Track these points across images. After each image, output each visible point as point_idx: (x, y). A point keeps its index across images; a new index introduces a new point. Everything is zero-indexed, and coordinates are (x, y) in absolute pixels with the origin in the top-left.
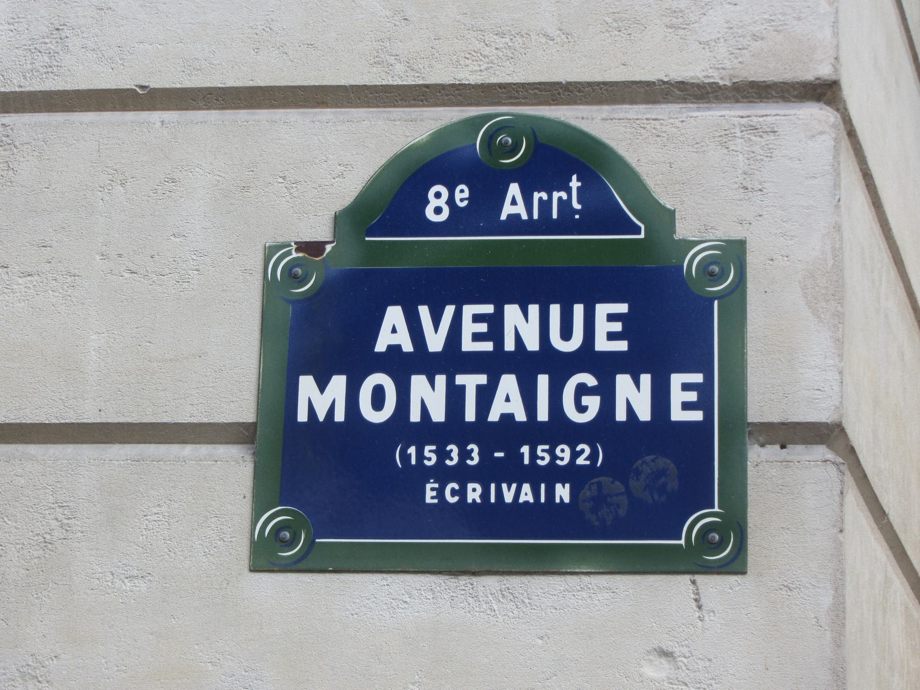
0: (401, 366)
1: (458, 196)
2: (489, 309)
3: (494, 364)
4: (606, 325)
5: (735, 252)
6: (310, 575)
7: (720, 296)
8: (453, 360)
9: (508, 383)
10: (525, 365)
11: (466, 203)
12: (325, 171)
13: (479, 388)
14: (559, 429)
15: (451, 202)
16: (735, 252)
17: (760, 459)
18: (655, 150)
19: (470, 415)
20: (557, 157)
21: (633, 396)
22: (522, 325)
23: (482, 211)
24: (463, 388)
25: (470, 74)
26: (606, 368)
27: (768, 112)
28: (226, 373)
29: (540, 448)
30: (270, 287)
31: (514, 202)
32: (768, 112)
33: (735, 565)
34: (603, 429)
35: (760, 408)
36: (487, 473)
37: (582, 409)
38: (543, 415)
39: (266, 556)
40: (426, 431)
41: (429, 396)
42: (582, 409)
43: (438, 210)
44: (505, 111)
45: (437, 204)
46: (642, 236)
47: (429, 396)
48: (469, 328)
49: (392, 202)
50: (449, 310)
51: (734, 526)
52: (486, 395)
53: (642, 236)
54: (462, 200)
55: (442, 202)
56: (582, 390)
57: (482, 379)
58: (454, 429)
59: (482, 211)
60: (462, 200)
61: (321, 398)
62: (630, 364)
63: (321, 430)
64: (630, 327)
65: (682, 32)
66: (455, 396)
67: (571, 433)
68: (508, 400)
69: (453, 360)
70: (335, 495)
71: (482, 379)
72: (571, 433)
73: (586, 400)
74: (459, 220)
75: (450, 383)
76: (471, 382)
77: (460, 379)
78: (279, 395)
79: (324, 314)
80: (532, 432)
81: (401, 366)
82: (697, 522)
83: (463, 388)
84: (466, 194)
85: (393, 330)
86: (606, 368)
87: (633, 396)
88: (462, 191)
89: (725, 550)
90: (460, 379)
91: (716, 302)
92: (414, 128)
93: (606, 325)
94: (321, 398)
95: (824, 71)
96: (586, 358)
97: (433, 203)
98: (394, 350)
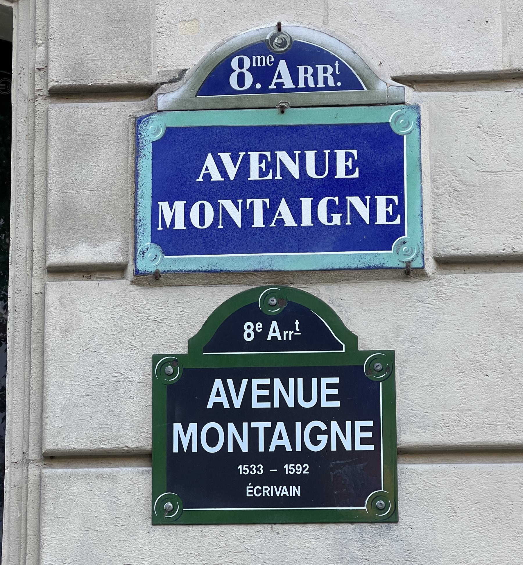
1: (257, 327)
2: (267, 381)
4: (324, 390)
6: (265, 529)
7: (383, 380)
9: (280, 426)
11: (261, 330)
13: (265, 429)
15: (254, 330)
19: (261, 449)
24: (327, 395)
29: (290, 465)
35: (406, 437)
37: (316, 443)
38: (298, 448)
42: (316, 443)
43: (249, 335)
45: (250, 331)
46: (344, 351)
48: (255, 393)
50: (245, 382)
52: (269, 433)
53: (344, 351)
54: (259, 329)
55: (251, 331)
56: (316, 431)
57: (269, 425)
60: (259, 329)
61: (186, 436)
63: (185, 456)
66: (253, 433)
71: (269, 425)
73: (319, 437)
75: (249, 425)
76: (261, 426)
77: (254, 425)
81: (222, 415)
83: (327, 395)
84: (261, 326)
85: (219, 394)
88: (259, 325)
90: (254, 425)
91: (381, 383)
93: (324, 390)
94: (186, 436)
95: (403, 100)
96: (318, 413)
97: (247, 331)
98: (218, 406)
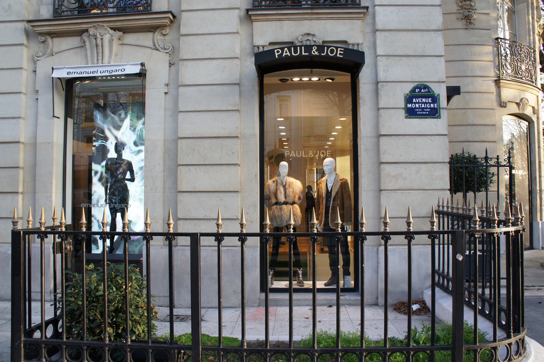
0: (415, 103)
3: (422, 103)
5: (439, 95)
8: (419, 103)
10: (424, 103)
12: (408, 88)
14: (427, 108)
16: (439, 95)
17: (441, 110)
18: (433, 86)
20: (426, 87)
21: (432, 105)
22: (424, 100)
23: (420, 91)
25: (418, 80)
26: (430, 103)
27: (538, 188)
28: (402, 104)
30: (405, 97)
31: (422, 91)
32: (538, 188)
33: (440, 118)
34: (430, 108)
36: (422, 111)
39: (406, 117)
40: (417, 108)
41: (417, 105)
44: (421, 83)
45: (417, 91)
47: (417, 105)
49: (413, 90)
51: (440, 115)
58: (419, 108)
59: (420, 91)
61: (409, 106)
62: (432, 103)
63: (409, 108)
64: (432, 100)
65: (287, 187)
67: (428, 108)
68: (423, 106)
69: (419, 103)
70: (411, 113)
72: (428, 108)
74: (419, 92)
78: (406, 106)
79: (409, 99)
80: (425, 108)
81: (415, 103)
82: (437, 115)
85: (414, 100)
86: (430, 103)
87: (432, 105)
89: (439, 117)
92: (416, 84)
94: (409, 106)
96: (428, 103)
